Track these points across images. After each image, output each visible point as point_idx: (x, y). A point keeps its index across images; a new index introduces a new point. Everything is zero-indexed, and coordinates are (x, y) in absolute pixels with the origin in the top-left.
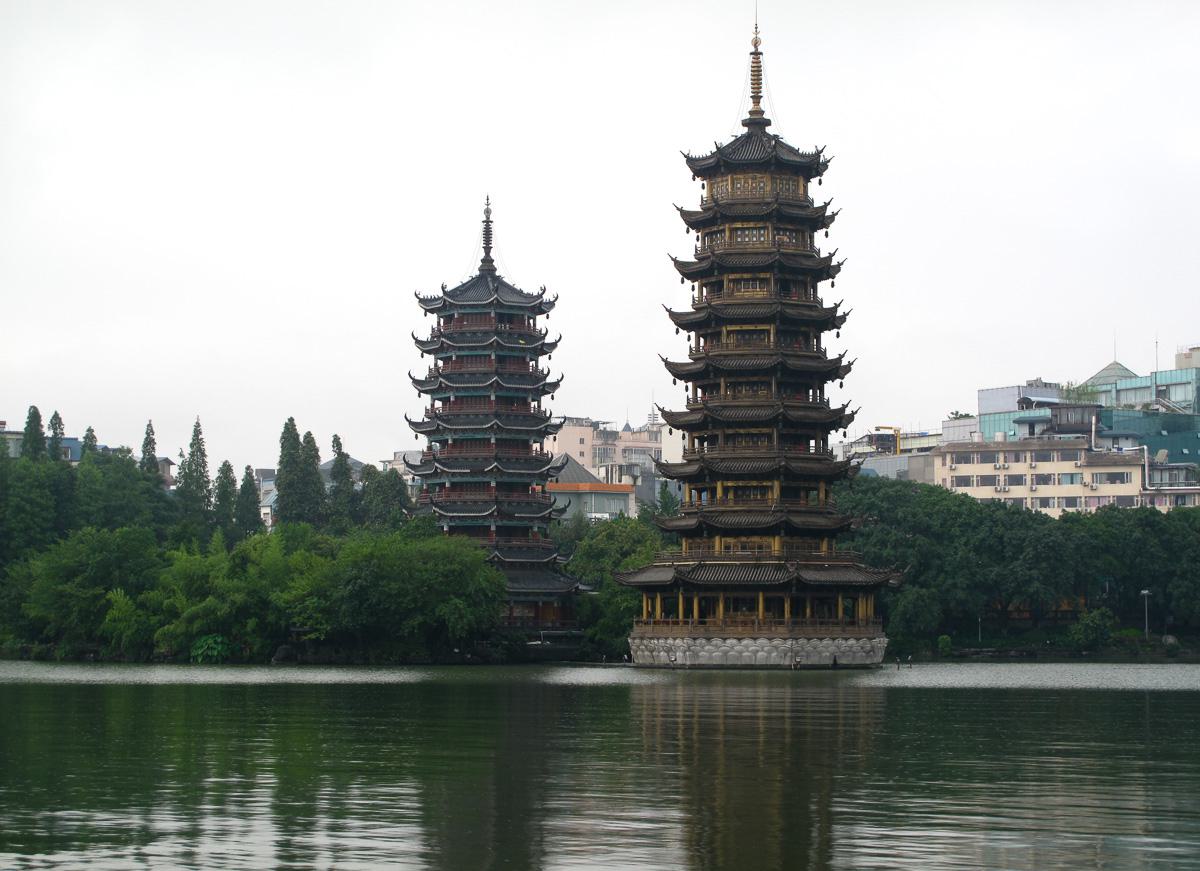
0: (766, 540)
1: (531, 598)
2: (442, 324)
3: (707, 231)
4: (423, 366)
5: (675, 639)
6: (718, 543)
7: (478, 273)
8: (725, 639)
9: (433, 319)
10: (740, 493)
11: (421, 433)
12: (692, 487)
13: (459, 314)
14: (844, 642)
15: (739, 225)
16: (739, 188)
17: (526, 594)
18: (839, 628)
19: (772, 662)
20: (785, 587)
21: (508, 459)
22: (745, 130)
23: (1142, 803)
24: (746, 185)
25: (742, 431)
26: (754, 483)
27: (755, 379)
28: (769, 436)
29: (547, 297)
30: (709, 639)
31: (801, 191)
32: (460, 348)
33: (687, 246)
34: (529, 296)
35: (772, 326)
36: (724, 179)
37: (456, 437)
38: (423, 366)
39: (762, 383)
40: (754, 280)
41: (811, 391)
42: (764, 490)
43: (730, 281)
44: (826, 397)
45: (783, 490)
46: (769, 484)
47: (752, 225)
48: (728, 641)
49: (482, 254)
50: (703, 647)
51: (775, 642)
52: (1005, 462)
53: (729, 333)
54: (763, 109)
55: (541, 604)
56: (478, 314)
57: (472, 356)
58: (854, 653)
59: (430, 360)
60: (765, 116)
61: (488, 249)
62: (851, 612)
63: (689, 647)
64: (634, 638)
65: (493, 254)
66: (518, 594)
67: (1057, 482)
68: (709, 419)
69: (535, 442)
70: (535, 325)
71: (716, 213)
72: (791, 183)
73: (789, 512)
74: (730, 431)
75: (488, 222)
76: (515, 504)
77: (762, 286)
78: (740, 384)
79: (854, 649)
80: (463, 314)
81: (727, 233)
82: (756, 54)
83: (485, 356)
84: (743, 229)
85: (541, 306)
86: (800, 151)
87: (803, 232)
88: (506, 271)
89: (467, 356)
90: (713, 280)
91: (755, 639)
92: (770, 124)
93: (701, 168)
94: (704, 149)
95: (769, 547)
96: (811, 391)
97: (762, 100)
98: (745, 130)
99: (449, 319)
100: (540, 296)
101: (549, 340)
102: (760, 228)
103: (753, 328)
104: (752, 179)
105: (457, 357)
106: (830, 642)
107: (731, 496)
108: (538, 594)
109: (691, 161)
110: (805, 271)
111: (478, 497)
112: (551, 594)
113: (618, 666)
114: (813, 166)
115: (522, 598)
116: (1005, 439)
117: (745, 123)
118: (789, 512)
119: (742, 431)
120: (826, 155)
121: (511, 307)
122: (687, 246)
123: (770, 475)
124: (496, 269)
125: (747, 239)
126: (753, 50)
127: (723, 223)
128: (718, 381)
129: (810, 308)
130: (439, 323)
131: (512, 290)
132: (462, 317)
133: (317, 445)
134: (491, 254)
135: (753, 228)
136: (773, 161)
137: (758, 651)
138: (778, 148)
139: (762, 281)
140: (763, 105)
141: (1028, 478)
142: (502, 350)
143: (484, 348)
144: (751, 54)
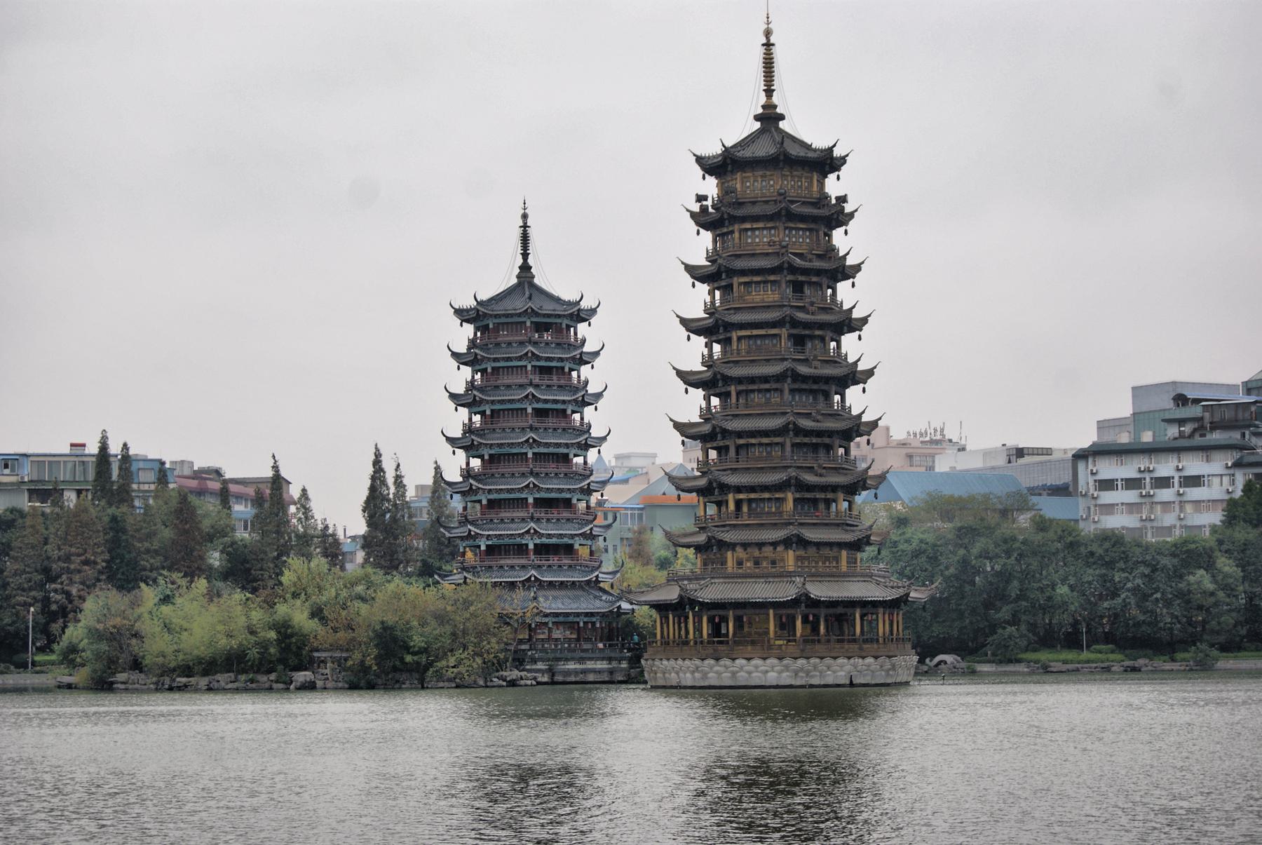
1: (571, 619)
3: (718, 232)
4: (461, 377)
5: (684, 660)
8: (734, 659)
9: (469, 330)
10: (754, 505)
11: (458, 448)
12: (706, 500)
14: (860, 660)
15: (748, 226)
16: (748, 187)
17: (567, 615)
18: (857, 646)
19: (782, 683)
20: (795, 603)
21: (547, 474)
22: (758, 125)
24: (756, 184)
25: (753, 441)
26: (766, 495)
27: (767, 386)
28: (782, 445)
30: (717, 659)
31: (815, 188)
32: (495, 360)
33: (699, 246)
34: (570, 303)
35: (784, 330)
36: (734, 177)
37: (492, 452)
38: (461, 377)
39: (776, 390)
40: (765, 282)
42: (828, 503)
43: (740, 284)
44: (848, 404)
45: (795, 500)
47: (761, 225)
48: (737, 661)
49: (520, 261)
50: (711, 668)
51: (785, 662)
52: (1179, 462)
53: (739, 338)
54: (777, 103)
55: (581, 624)
56: (511, 322)
57: (508, 367)
58: (873, 672)
59: (467, 372)
60: (778, 110)
61: (525, 255)
63: (697, 668)
64: (646, 660)
65: (531, 261)
66: (557, 615)
68: (718, 430)
69: (575, 456)
71: (723, 214)
72: (803, 180)
73: (801, 524)
74: (741, 441)
76: (554, 521)
77: (773, 288)
78: (753, 391)
79: (873, 667)
80: (498, 324)
81: (736, 235)
82: (768, 45)
83: (521, 367)
84: (753, 230)
85: (581, 315)
86: (813, 146)
87: (817, 231)
89: (503, 367)
90: (723, 283)
91: (764, 659)
93: (716, 166)
94: (713, 149)
95: (783, 560)
97: (774, 93)
98: (758, 125)
99: (483, 329)
100: (578, 303)
101: (588, 348)
102: (770, 228)
104: (762, 176)
106: (846, 661)
108: (578, 615)
109: (700, 160)
111: (515, 514)
112: (592, 614)
113: (20, 690)
114: (828, 163)
115: (561, 619)
116: (1154, 439)
117: (757, 118)
118: (801, 524)
119: (753, 441)
120: (837, 152)
121: (549, 316)
122: (699, 246)
123: (781, 487)
124: (533, 277)
125: (757, 240)
126: (764, 41)
127: (731, 224)
128: (729, 389)
129: (825, 310)
132: (498, 327)
134: (529, 260)
135: (763, 229)
137: (767, 672)
138: (787, 143)
139: (773, 282)
140: (776, 99)
141: (1176, 480)
142: (538, 360)
143: (520, 359)
144: (763, 45)
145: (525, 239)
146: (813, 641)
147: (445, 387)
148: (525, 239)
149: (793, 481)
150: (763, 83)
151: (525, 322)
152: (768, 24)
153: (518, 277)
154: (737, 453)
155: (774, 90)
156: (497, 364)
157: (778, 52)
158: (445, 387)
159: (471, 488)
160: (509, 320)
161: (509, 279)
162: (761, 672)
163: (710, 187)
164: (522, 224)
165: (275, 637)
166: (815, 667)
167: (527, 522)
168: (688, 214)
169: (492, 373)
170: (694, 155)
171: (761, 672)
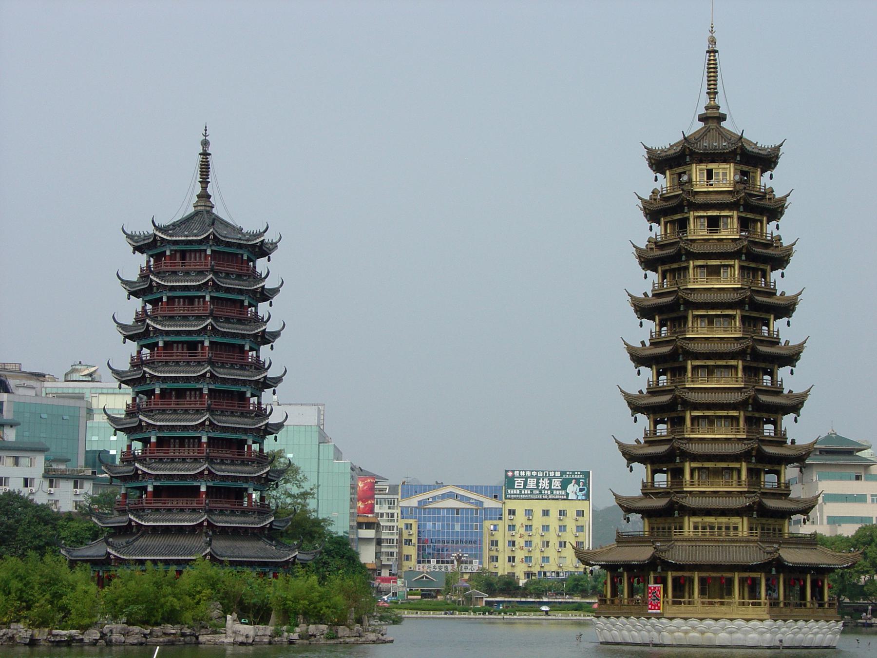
0: (736, 520)
2: (152, 263)
6: (689, 523)
13: (171, 251)
29: (268, 237)
49: (198, 189)
56: (184, 251)
60: (721, 111)
61: (205, 182)
62: (546, 594)
70: (255, 267)
75: (205, 154)
80: (176, 251)
85: (263, 250)
100: (261, 234)
103: (758, 316)
105: (168, 298)
107: (696, 475)
117: (702, 118)
130: (148, 262)
131: (226, 225)
136: (739, 151)
143: (240, 292)
146: (801, 605)
147: (113, 317)
149: (754, 453)
151: (205, 250)
152: (206, 136)
154: (692, 424)
155: (209, 182)
157: (722, 59)
158: (114, 317)
159: (140, 424)
161: (187, 208)
162: (682, 631)
164: (201, 151)
165: (521, 585)
167: (200, 462)
168: (639, 202)
169: (168, 303)
170: (646, 148)
171: (682, 631)
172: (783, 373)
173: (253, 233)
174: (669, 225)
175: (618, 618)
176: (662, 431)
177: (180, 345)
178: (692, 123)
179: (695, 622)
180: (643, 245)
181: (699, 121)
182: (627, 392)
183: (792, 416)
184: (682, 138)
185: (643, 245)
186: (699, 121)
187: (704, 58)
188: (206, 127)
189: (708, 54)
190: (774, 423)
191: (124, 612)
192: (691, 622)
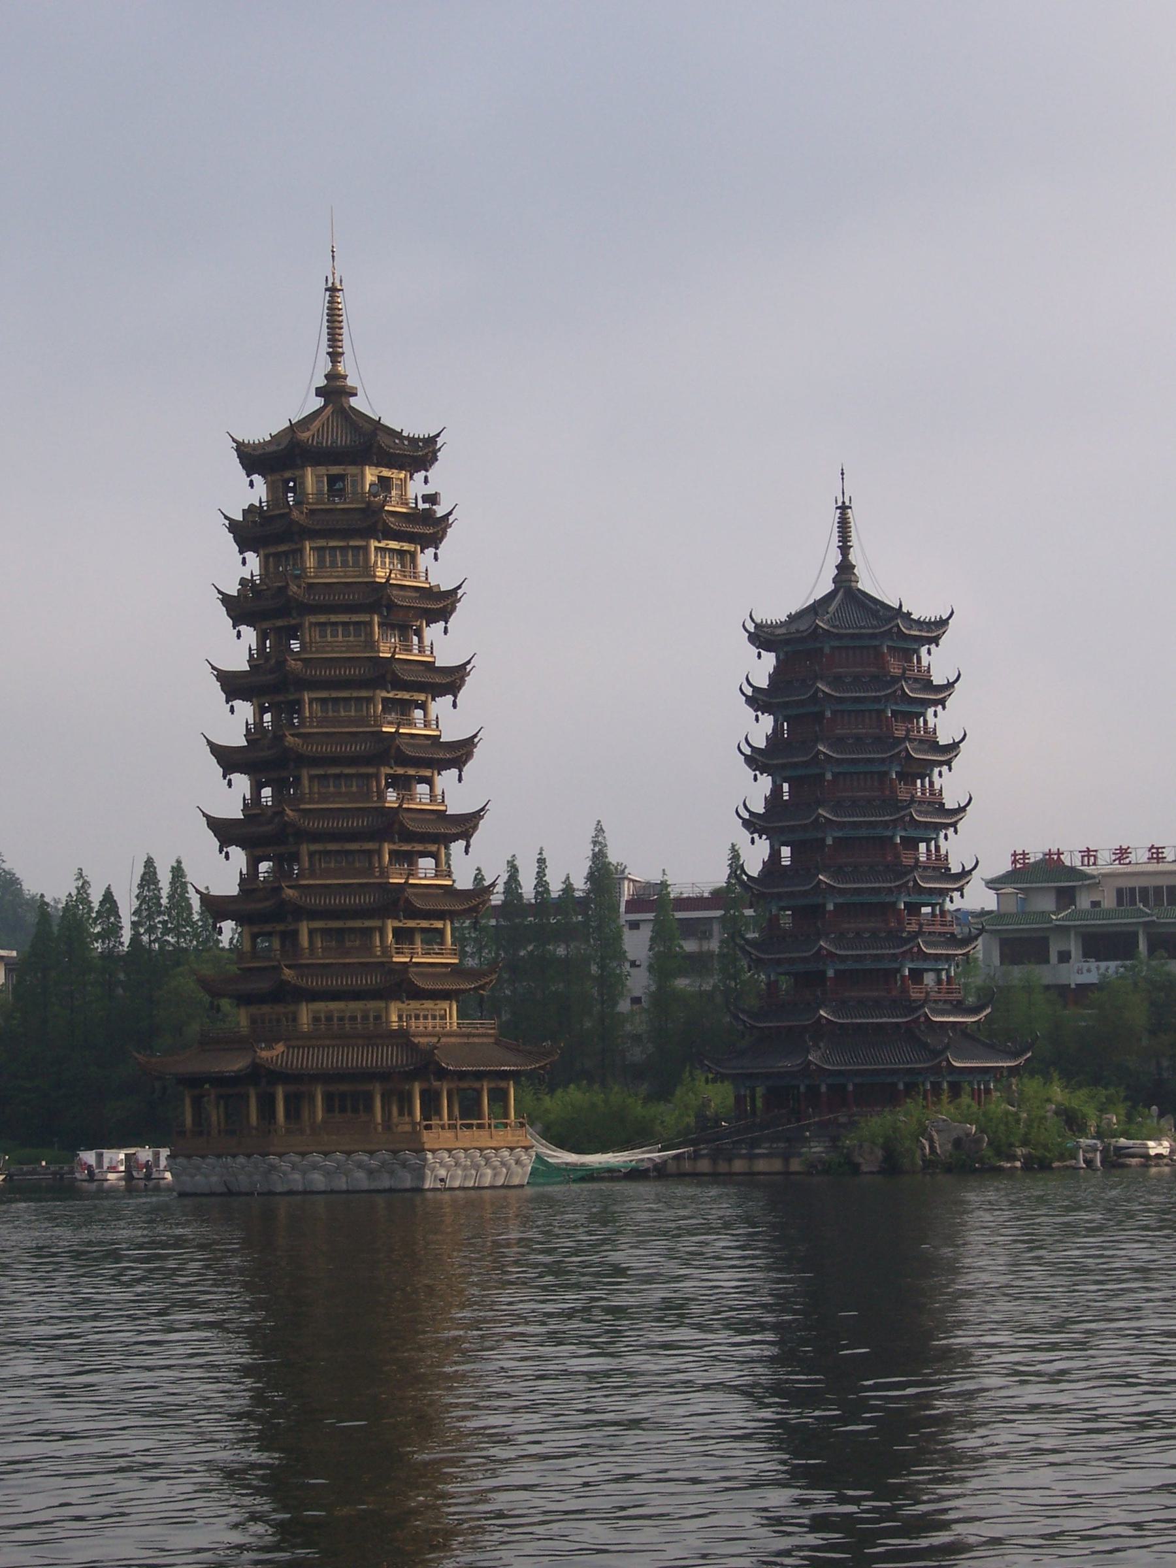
7: (833, 587)
22: (320, 402)
23: (56, 1282)
41: (919, 781)
42: (367, 932)
46: (364, 543)
49: (835, 557)
60: (350, 382)
61: (845, 549)
65: (852, 558)
67: (1151, 892)
88: (866, 583)
92: (356, 395)
96: (919, 781)
98: (320, 402)
110: (446, 617)
117: (319, 392)
133: (115, 898)
134: (850, 557)
145: (844, 526)
148: (844, 526)
150: (837, 539)
153: (835, 581)
155: (851, 547)
156: (839, 707)
160: (857, 643)
163: (258, 492)
166: (198, 1168)
172: (446, 780)
173: (930, 619)
174: (271, 559)
175: (203, 1157)
176: (428, 871)
177: (862, 777)
178: (306, 398)
179: (317, 1158)
180: (233, 590)
181: (317, 395)
182: (209, 814)
183: (461, 843)
184: (288, 424)
185: (233, 590)
186: (317, 395)
187: (321, 301)
188: (842, 470)
189: (328, 293)
190: (435, 856)
191: (51, 1174)
192: (358, 1157)
